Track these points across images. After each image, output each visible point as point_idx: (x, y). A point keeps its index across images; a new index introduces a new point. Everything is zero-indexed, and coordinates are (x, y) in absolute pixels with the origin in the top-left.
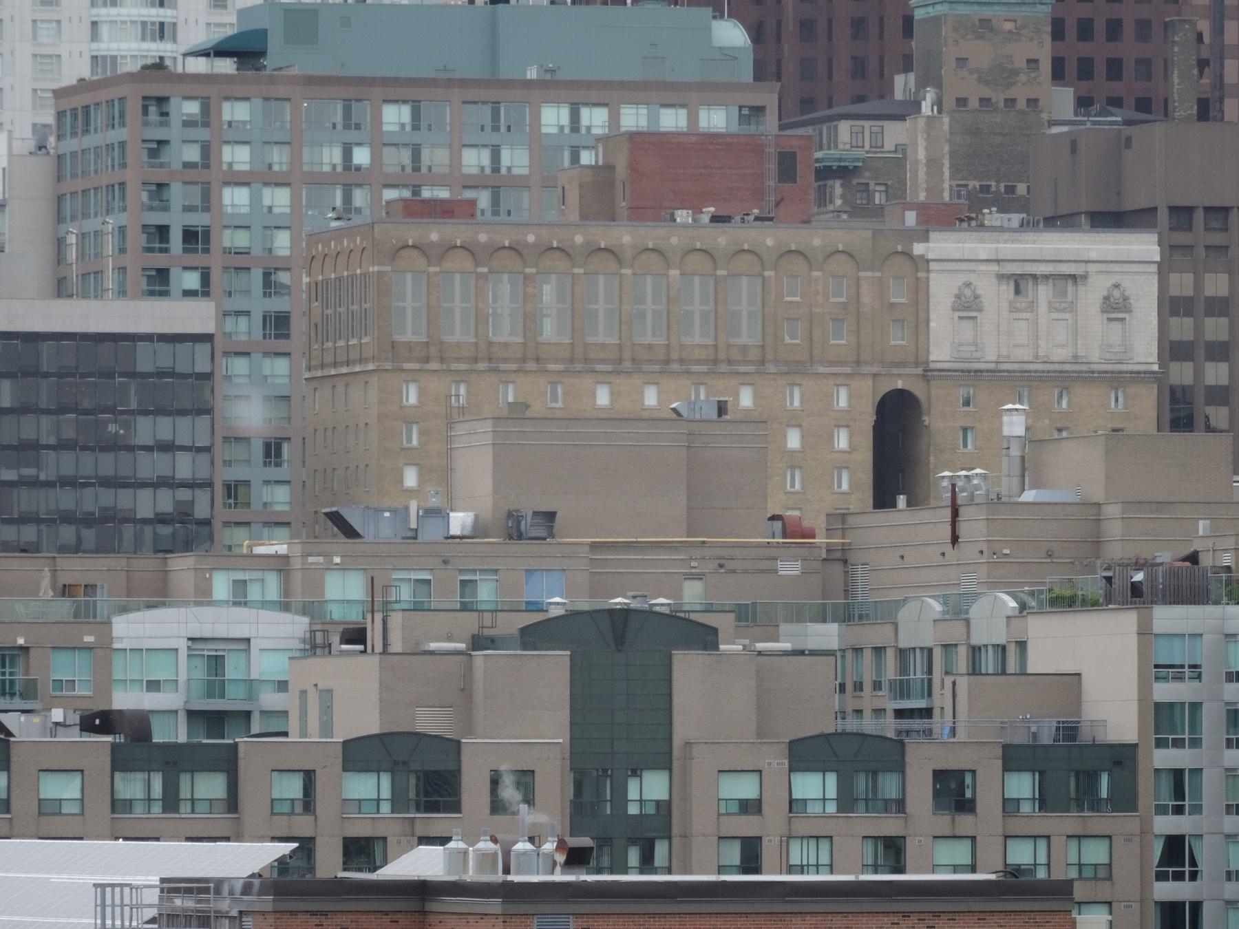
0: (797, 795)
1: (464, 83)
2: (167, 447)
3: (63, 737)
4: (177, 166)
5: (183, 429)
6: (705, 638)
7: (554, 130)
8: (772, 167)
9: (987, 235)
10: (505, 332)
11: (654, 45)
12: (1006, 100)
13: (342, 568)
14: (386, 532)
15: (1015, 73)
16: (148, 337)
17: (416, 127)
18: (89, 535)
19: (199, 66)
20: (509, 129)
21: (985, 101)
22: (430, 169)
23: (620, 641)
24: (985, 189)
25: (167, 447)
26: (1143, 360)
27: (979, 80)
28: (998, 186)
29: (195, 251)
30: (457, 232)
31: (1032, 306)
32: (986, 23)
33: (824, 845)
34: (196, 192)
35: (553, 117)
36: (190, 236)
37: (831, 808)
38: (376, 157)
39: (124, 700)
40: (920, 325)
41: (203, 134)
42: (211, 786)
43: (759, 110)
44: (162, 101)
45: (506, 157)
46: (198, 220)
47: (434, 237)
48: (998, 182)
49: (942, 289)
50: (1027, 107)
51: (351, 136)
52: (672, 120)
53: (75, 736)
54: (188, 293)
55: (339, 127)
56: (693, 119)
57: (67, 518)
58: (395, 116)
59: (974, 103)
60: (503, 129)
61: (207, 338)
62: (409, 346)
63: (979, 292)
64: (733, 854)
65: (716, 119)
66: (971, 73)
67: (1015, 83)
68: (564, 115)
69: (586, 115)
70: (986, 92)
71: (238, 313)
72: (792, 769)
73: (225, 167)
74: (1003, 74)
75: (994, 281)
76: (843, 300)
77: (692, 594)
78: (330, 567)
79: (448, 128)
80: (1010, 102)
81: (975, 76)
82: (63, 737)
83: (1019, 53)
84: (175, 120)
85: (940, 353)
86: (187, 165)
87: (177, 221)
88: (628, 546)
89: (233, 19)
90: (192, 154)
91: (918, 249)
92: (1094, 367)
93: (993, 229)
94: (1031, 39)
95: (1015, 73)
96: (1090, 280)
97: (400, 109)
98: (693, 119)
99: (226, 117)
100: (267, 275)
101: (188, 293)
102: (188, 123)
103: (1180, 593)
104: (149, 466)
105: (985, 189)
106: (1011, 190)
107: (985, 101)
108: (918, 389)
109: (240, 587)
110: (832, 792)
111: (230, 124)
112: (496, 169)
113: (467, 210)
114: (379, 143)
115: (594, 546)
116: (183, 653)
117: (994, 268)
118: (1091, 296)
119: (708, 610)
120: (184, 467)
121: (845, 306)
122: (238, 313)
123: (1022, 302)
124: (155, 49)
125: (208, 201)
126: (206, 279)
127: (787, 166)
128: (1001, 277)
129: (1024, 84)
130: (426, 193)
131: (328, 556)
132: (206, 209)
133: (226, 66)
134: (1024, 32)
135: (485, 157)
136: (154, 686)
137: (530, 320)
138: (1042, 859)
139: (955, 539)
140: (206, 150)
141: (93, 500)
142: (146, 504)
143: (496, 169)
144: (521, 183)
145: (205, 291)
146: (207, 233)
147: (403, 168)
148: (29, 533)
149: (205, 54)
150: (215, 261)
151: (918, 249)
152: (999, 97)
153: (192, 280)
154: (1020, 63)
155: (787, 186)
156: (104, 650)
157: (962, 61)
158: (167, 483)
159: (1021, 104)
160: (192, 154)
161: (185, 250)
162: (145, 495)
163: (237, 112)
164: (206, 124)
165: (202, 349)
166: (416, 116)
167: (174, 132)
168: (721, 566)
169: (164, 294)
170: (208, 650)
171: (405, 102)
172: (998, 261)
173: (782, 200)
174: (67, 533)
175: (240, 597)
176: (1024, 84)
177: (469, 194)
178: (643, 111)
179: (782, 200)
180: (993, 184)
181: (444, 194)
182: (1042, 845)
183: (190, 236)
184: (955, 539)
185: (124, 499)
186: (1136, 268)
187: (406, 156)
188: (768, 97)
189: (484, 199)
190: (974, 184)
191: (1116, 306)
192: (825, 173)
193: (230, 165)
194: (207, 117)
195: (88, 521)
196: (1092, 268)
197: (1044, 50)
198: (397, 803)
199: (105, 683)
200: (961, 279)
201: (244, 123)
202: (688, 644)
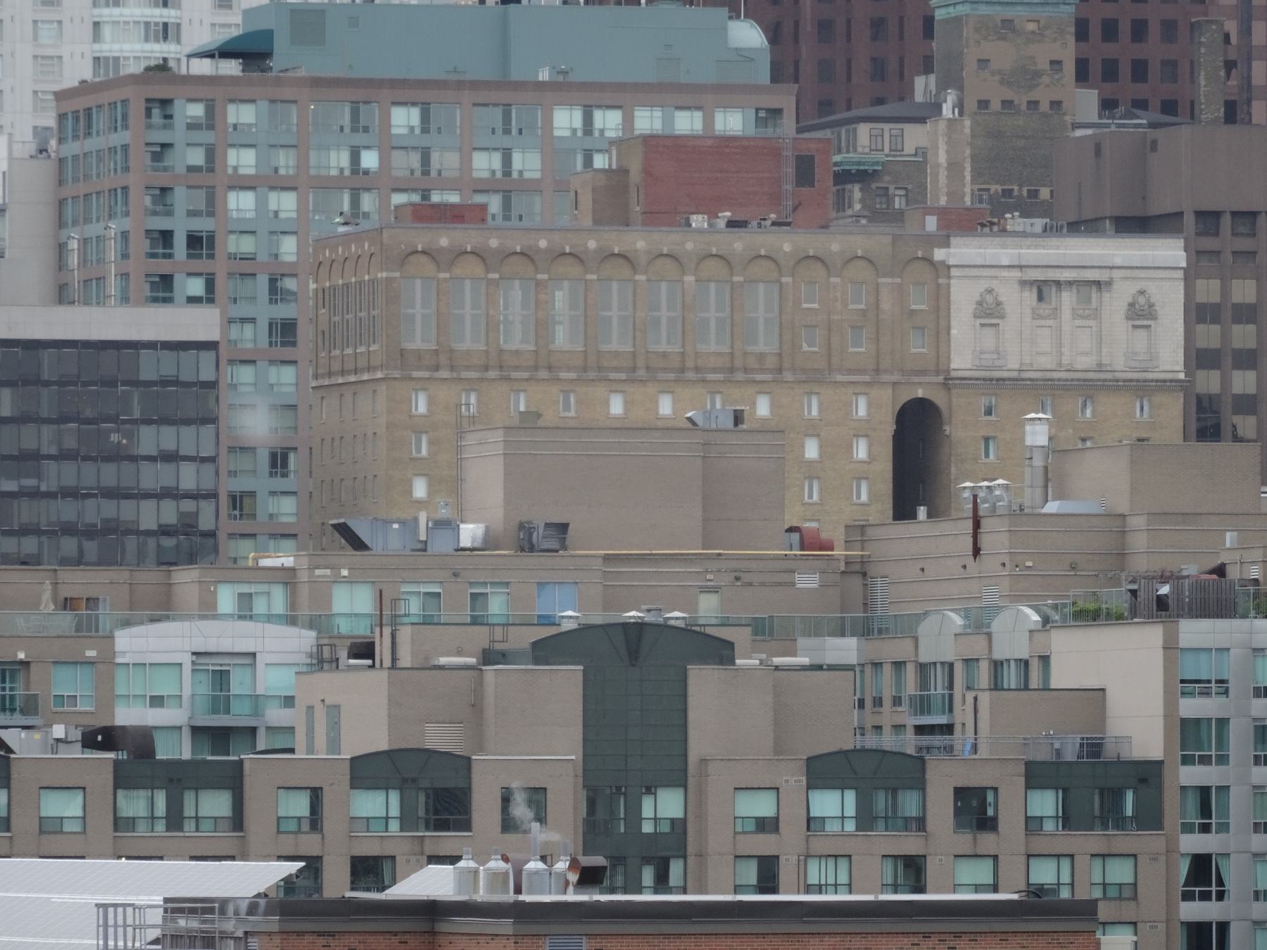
0: (815, 813)
1: (475, 85)
2: (171, 457)
3: (65, 754)
4: (181, 169)
5: (187, 439)
6: (721, 652)
7: (567, 133)
8: (790, 170)
9: (1009, 240)
10: (516, 340)
11: (669, 46)
12: (1029, 103)
13: (350, 581)
14: (395, 544)
15: (1038, 74)
16: (152, 345)
17: (425, 130)
18: (91, 547)
19: (203, 67)
20: (520, 131)
21: (1007, 104)
22: (440, 173)
23: (634, 655)
24: (1007, 193)
25: (171, 457)
26: (1169, 368)
27: (1002, 82)
28: (1020, 190)
29: (200, 256)
30: (468, 237)
31: (1056, 313)
32: (1008, 23)
33: (843, 864)
34: (200, 197)
35: (566, 120)
36: (194, 241)
37: (850, 826)
38: (384, 160)
39: (127, 716)
40: (940, 332)
41: (207, 137)
42: (216, 804)
43: (776, 113)
44: (165, 103)
45: (517, 161)
46: (202, 225)
47: (444, 242)
48: (1021, 186)
49: (963, 296)
50: (1050, 109)
51: (359, 139)
52: (687, 123)
53: (76, 753)
54: (193, 300)
55: (347, 130)
56: (709, 122)
57: (69, 530)
58: (404, 119)
59: (996, 105)
60: (514, 131)
61: (211, 346)
62: (418, 354)
63: (1002, 299)
64: (750, 874)
65: (732, 122)
66: (993, 75)
67: (1038, 85)
68: (577, 118)
69: (599, 117)
70: (1009, 94)
71: (244, 320)
72: (810, 787)
73: (230, 171)
74: (1026, 76)
75: (1017, 287)
76: (862, 306)
77: (708, 608)
78: (338, 580)
79: (458, 131)
80: (1033, 104)
81: (997, 78)
82: (65, 754)
83: (1042, 54)
84: (179, 122)
85: (961, 361)
86: (192, 169)
87: (181, 226)
88: (642, 559)
89: (238, 19)
90: (197, 157)
91: (939, 254)
92: (1118, 375)
93: (1016, 234)
94: (1055, 40)
95: (1038, 74)
96: (1115, 286)
97: (409, 111)
98: (709, 122)
99: (231, 119)
100: (273, 281)
101: (193, 300)
102: (193, 126)
103: (1207, 606)
104: (152, 476)
105: (1007, 193)
106: (1034, 194)
107: (1007, 104)
108: (939, 398)
109: (245, 600)
110: (851, 810)
111: (235, 127)
112: (507, 173)
113: (478, 214)
114: (387, 146)
115: (608, 559)
116: (187, 668)
117: (1017, 274)
118: (1115, 303)
119: (724, 624)
120: (188, 477)
121: (864, 313)
122: (244, 320)
123: (1045, 309)
124: (158, 50)
125: (212, 206)
126: (210, 285)
127: (805, 170)
128: (1023, 283)
129: (1048, 86)
130: (436, 198)
131: (335, 568)
132: (211, 214)
133: (231, 68)
134: (1047, 32)
135: (496, 161)
136: (157, 701)
137: (542, 328)
138: (1065, 878)
139: (976, 551)
140: (211, 153)
141: (95, 512)
142: (149, 515)
143: (507, 173)
144: (533, 187)
145: (209, 297)
146: (211, 238)
147: (412, 172)
148: (30, 545)
149: (210, 55)
150: (220, 267)
151: (939, 254)
152: (1021, 100)
153: (196, 287)
154: (1043, 65)
155: (805, 190)
156: (106, 665)
157: (983, 63)
158: (171, 493)
159: (1044, 107)
160: (197, 157)
161: (189, 256)
162: (148, 506)
163: (242, 114)
164: (211, 127)
165: (207, 357)
166: (425, 118)
167: (178, 135)
168: (737, 579)
169: (168, 300)
170: (212, 664)
171: (414, 104)
172: (1021, 267)
173: (800, 204)
174: (69, 545)
175: (245, 611)
176: (1048, 86)
177: (479, 199)
178: (658, 113)
179: (800, 204)
180: (1016, 188)
181: (454, 198)
182: (1065, 864)
183: (194, 241)
184: (976, 551)
185: (127, 510)
186: (1161, 274)
187: (415, 160)
188: (786, 100)
189: (495, 204)
190: (996, 188)
191: (1141, 313)
192: (843, 177)
193: (235, 168)
194: (212, 120)
195: (90, 533)
196: (1116, 274)
197: (1067, 51)
198: (406, 821)
199: (107, 698)
200: (983, 285)
201: (250, 125)
202: (703, 659)
